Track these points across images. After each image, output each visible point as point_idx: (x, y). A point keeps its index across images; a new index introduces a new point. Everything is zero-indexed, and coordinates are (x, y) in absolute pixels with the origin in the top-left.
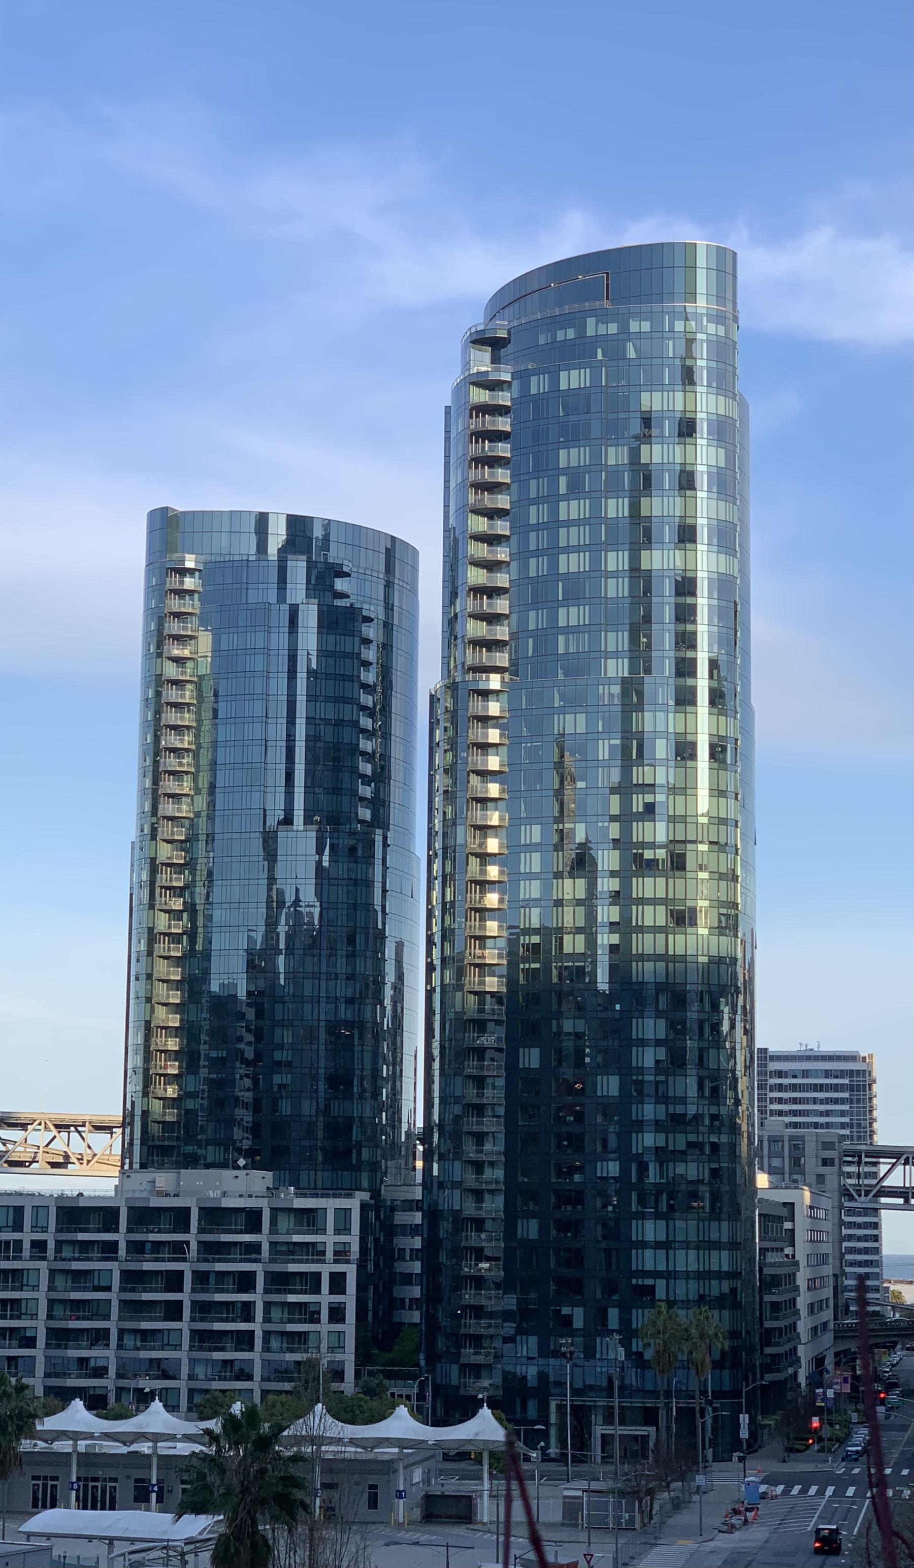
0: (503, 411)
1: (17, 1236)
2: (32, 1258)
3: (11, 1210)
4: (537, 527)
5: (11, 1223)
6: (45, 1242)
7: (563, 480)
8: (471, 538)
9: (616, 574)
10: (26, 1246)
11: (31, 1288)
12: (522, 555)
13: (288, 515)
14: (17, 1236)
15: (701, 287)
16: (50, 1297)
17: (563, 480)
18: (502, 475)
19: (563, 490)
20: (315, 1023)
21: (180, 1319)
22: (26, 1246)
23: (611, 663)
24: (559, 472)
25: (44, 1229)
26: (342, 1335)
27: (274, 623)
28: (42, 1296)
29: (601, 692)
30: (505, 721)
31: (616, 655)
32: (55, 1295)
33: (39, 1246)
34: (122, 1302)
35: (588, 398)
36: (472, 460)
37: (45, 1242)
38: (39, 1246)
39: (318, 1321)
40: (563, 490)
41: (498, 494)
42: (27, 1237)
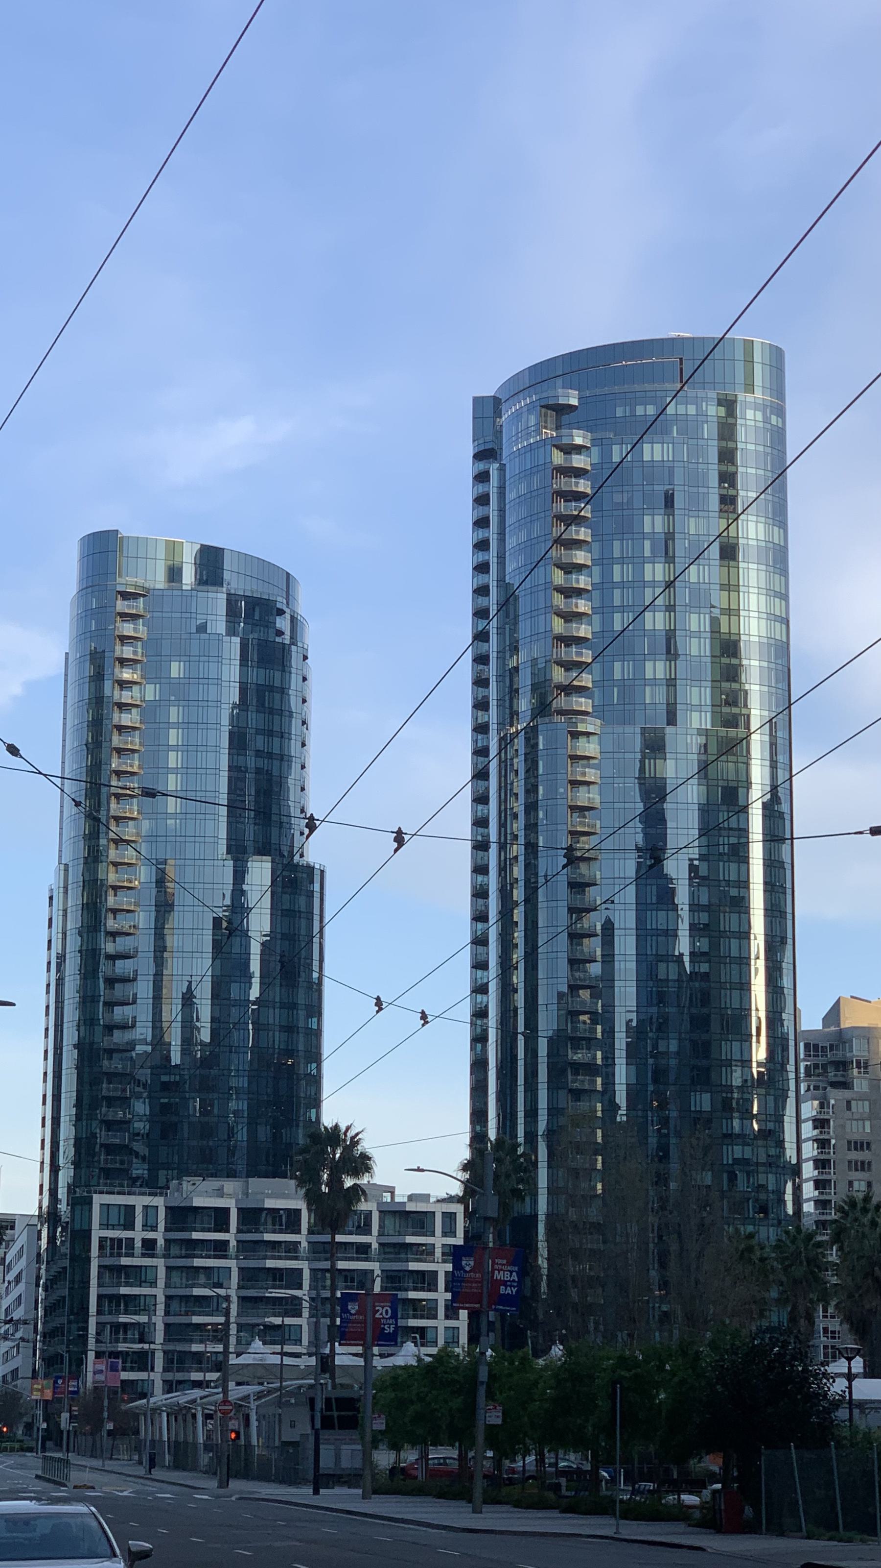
0: (579, 473)
1: (128, 1234)
2: (144, 1255)
3: (122, 1209)
4: (622, 585)
5: (122, 1222)
6: (155, 1241)
7: (647, 544)
8: (554, 589)
9: (698, 634)
10: (138, 1244)
11: (148, 1284)
12: (604, 610)
13: (202, 545)
14: (128, 1234)
15: (758, 381)
16: (168, 1294)
17: (647, 544)
18: (583, 534)
19: (647, 553)
20: (271, 1051)
21: (300, 1315)
22: (138, 1244)
23: (695, 715)
24: (644, 536)
25: (154, 1228)
26: (456, 1331)
27: (226, 655)
28: (159, 1292)
29: (689, 741)
30: (596, 761)
31: (699, 708)
32: (172, 1292)
33: (149, 1245)
34: (242, 1300)
35: (671, 470)
36: (555, 516)
37: (155, 1241)
38: (149, 1245)
39: (435, 1317)
40: (647, 553)
41: (577, 549)
42: (138, 1235)
